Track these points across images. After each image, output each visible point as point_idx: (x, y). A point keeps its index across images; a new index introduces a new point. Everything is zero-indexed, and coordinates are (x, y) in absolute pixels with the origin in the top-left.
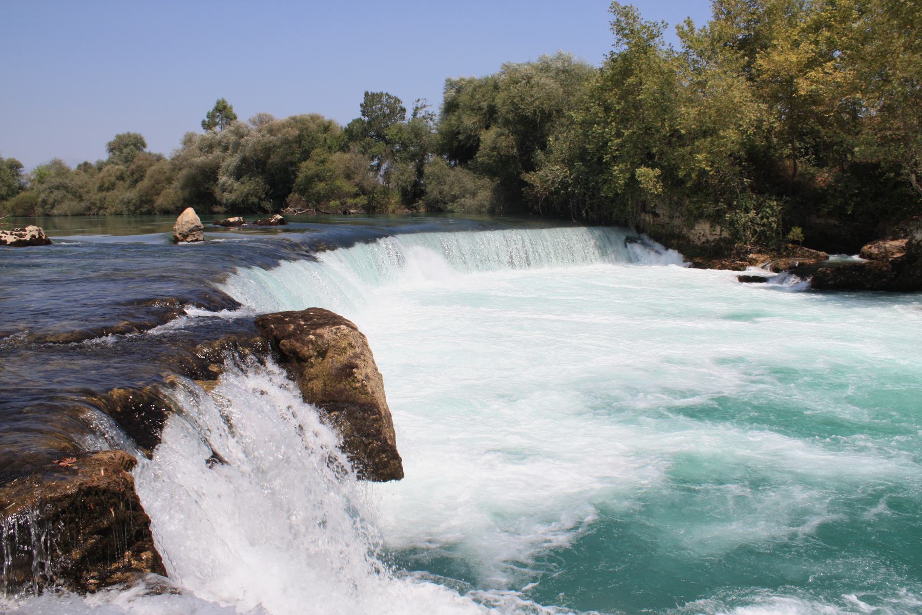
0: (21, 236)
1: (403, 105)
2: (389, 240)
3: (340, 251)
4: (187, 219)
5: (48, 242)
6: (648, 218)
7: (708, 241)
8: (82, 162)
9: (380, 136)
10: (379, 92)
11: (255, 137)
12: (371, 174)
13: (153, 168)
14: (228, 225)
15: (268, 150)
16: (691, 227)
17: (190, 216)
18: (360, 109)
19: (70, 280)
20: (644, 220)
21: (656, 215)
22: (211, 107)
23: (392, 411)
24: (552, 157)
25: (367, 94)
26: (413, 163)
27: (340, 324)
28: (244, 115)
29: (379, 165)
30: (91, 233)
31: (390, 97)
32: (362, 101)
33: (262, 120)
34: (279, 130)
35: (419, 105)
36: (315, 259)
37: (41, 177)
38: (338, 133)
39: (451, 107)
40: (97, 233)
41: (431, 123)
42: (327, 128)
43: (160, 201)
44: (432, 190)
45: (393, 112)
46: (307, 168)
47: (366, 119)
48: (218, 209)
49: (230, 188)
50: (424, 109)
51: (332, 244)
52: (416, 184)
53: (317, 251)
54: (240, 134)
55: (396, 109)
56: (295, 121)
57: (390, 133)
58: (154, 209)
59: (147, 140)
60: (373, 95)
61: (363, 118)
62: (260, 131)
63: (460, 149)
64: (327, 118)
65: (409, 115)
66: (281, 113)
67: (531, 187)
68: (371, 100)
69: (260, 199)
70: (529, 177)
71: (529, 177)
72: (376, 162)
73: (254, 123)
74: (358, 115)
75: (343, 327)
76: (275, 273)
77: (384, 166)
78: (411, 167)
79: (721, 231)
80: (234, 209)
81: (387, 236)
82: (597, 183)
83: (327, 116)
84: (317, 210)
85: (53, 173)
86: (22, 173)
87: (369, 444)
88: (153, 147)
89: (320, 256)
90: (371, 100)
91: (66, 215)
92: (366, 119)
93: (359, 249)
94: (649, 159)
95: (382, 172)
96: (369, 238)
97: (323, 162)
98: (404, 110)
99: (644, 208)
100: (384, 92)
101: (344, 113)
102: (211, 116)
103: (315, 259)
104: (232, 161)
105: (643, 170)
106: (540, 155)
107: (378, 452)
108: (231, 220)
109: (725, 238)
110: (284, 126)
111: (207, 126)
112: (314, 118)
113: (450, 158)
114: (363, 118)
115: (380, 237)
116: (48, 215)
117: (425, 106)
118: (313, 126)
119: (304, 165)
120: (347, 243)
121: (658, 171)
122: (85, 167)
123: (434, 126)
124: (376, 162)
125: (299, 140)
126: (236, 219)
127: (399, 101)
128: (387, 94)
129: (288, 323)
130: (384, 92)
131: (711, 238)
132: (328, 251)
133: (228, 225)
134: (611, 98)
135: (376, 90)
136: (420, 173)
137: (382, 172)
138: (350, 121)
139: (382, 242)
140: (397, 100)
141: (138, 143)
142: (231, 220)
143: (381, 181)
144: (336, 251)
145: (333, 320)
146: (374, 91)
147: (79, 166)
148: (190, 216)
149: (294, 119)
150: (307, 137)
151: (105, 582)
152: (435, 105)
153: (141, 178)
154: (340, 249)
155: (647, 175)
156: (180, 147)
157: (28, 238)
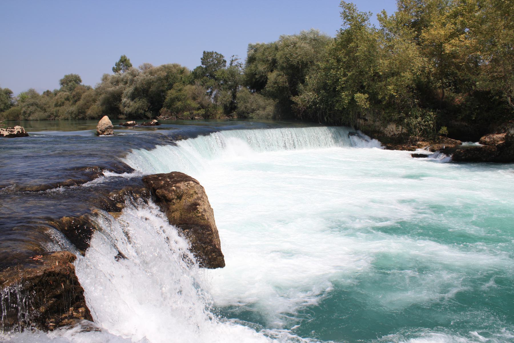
0: (12, 131)
1: (225, 59)
2: (217, 134)
3: (190, 140)
4: (104, 122)
5: (27, 135)
6: (361, 122)
7: (395, 134)
9: (212, 76)
11: (142, 77)
12: (207, 97)
14: (127, 125)
15: (150, 84)
16: (385, 127)
17: (106, 120)
18: (200, 60)
19: (39, 156)
20: (359, 123)
21: (366, 120)
22: (117, 60)
24: (308, 87)
25: (204, 52)
26: (230, 91)
27: (190, 181)
28: (136, 64)
29: (211, 92)
30: (51, 130)
31: (217, 54)
32: (202, 57)
33: (146, 67)
34: (155, 72)
35: (234, 58)
36: (175, 145)
37: (23, 99)
38: (189, 74)
39: (251, 60)
41: (240, 69)
42: (182, 71)
43: (89, 112)
44: (241, 106)
46: (171, 94)
47: (204, 66)
48: (121, 116)
49: (128, 105)
51: (185, 136)
52: (232, 103)
53: (177, 140)
54: (134, 75)
55: (221, 61)
56: (165, 68)
57: (218, 74)
58: (86, 116)
59: (82, 78)
60: (208, 53)
61: (202, 66)
62: (145, 73)
63: (256, 83)
64: (182, 66)
65: (228, 64)
66: (157, 63)
67: (296, 104)
68: (207, 56)
69: (145, 111)
70: (295, 99)
71: (295, 99)
72: (209, 90)
73: (142, 69)
74: (199, 64)
75: (191, 182)
76: (153, 152)
77: (214, 93)
78: (229, 93)
79: (402, 129)
80: (130, 116)
81: (215, 132)
82: (333, 102)
83: (182, 64)
85: (29, 96)
86: (13, 97)
88: (85, 82)
89: (178, 143)
90: (207, 56)
92: (204, 66)
93: (200, 139)
94: (362, 89)
95: (213, 96)
96: (206, 133)
97: (180, 90)
98: (225, 61)
99: (359, 116)
100: (214, 52)
101: (192, 63)
102: (118, 65)
103: (175, 145)
104: (129, 90)
105: (358, 95)
106: (301, 86)
108: (129, 123)
109: (404, 133)
110: (158, 70)
111: (115, 70)
112: (175, 66)
113: (251, 88)
114: (202, 66)
115: (212, 132)
116: (27, 120)
117: (237, 59)
118: (174, 71)
119: (169, 92)
120: (193, 135)
121: (367, 96)
122: (48, 93)
123: (242, 70)
124: (209, 90)
125: (167, 78)
126: (132, 122)
128: (216, 52)
129: (161, 180)
130: (214, 52)
131: (396, 133)
132: (183, 140)
134: (341, 54)
135: (210, 50)
136: (234, 96)
137: (213, 96)
138: (195, 68)
139: (213, 135)
140: (221, 56)
141: (77, 80)
142: (129, 123)
144: (187, 140)
147: (44, 93)
148: (106, 120)
150: (171, 76)
151: (58, 325)
152: (243, 58)
153: (79, 99)
154: (190, 139)
155: (361, 98)
157: (15, 133)
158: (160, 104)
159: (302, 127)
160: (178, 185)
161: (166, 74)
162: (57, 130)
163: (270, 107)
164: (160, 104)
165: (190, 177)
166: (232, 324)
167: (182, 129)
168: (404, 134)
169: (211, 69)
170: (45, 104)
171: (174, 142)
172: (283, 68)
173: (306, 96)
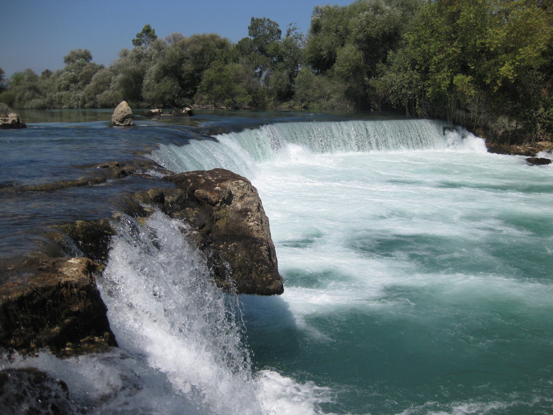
0: (5, 120)
1: (280, 28)
2: (268, 127)
3: (232, 135)
4: (122, 110)
5: (24, 126)
6: (461, 113)
7: (506, 132)
8: (44, 71)
9: (262, 51)
10: (262, 18)
12: (255, 80)
13: (97, 74)
14: (152, 115)
16: (494, 121)
17: (123, 107)
18: (248, 30)
19: (44, 151)
20: (459, 115)
21: (468, 111)
22: (140, 31)
23: (275, 244)
24: (391, 68)
25: (253, 19)
26: (286, 71)
27: (239, 179)
28: (163, 34)
29: (261, 73)
30: (52, 121)
31: (270, 22)
32: (250, 25)
34: (188, 45)
35: (291, 28)
36: (215, 140)
37: (18, 79)
38: (231, 49)
39: (316, 28)
40: (57, 121)
41: (300, 42)
42: (223, 45)
43: (100, 98)
44: (299, 90)
45: (272, 32)
47: (252, 38)
48: (144, 104)
49: (150, 87)
50: (295, 31)
51: (226, 130)
52: (289, 87)
53: (216, 134)
54: (159, 48)
56: (197, 40)
57: (270, 49)
58: (96, 103)
59: (92, 54)
60: (258, 20)
61: (249, 37)
62: (175, 46)
65: (283, 35)
66: (187, 34)
67: (374, 89)
69: (174, 96)
70: (371, 82)
71: (371, 82)
72: (258, 70)
73: (170, 41)
75: (240, 181)
76: (186, 148)
77: (265, 73)
78: (285, 73)
79: (517, 124)
80: (153, 103)
81: (267, 124)
82: (424, 86)
83: (223, 34)
84: (215, 106)
85: (26, 77)
86: (5, 78)
87: (259, 267)
88: (96, 60)
89: (219, 137)
90: (256, 25)
91: (32, 109)
92: (252, 38)
93: (246, 134)
94: (465, 70)
95: (263, 77)
96: (256, 125)
98: (280, 32)
99: (459, 106)
100: (266, 18)
102: (140, 36)
103: (215, 140)
104: (153, 68)
105: (460, 77)
106: (380, 65)
107: (266, 273)
108: (153, 111)
109: (520, 129)
111: (137, 43)
112: (213, 37)
113: (314, 68)
114: (249, 37)
115: (262, 125)
116: (21, 109)
117: (296, 29)
118: (212, 43)
120: (238, 129)
121: (470, 78)
122: (47, 73)
123: (303, 45)
124: (258, 70)
126: (157, 110)
127: (277, 25)
128: (268, 20)
129: (201, 178)
130: (266, 18)
131: (509, 129)
132: (224, 134)
133: (152, 115)
134: (438, 21)
135: (260, 17)
136: (292, 76)
137: (263, 77)
138: (240, 39)
139: (263, 128)
141: (87, 56)
142: (153, 111)
143: (262, 84)
144: (230, 134)
145: (235, 177)
146: (259, 18)
147: (43, 73)
148: (123, 107)
149: (198, 37)
150: (209, 51)
151: (77, 352)
152: (304, 29)
153: (87, 82)
154: (233, 133)
155: (461, 80)
156: (118, 58)
157: (10, 122)
158: (204, 86)
159: (382, 120)
160: (224, 184)
161: (201, 47)
162: (61, 121)
163: (332, 87)
164: (204, 86)
165: (239, 176)
166: (317, 17)
167: (225, 121)
168: (520, 131)
169: (263, 42)
170: (45, 88)
171: (213, 136)
172: (358, 41)
173: (392, 78)
